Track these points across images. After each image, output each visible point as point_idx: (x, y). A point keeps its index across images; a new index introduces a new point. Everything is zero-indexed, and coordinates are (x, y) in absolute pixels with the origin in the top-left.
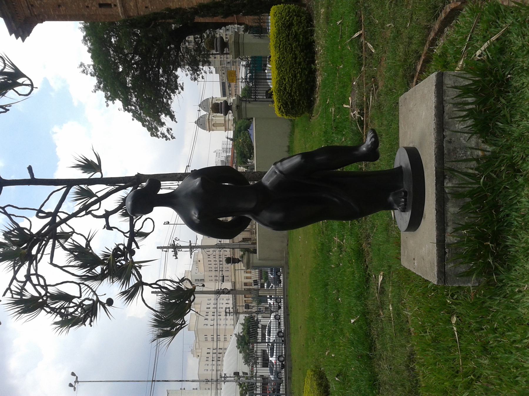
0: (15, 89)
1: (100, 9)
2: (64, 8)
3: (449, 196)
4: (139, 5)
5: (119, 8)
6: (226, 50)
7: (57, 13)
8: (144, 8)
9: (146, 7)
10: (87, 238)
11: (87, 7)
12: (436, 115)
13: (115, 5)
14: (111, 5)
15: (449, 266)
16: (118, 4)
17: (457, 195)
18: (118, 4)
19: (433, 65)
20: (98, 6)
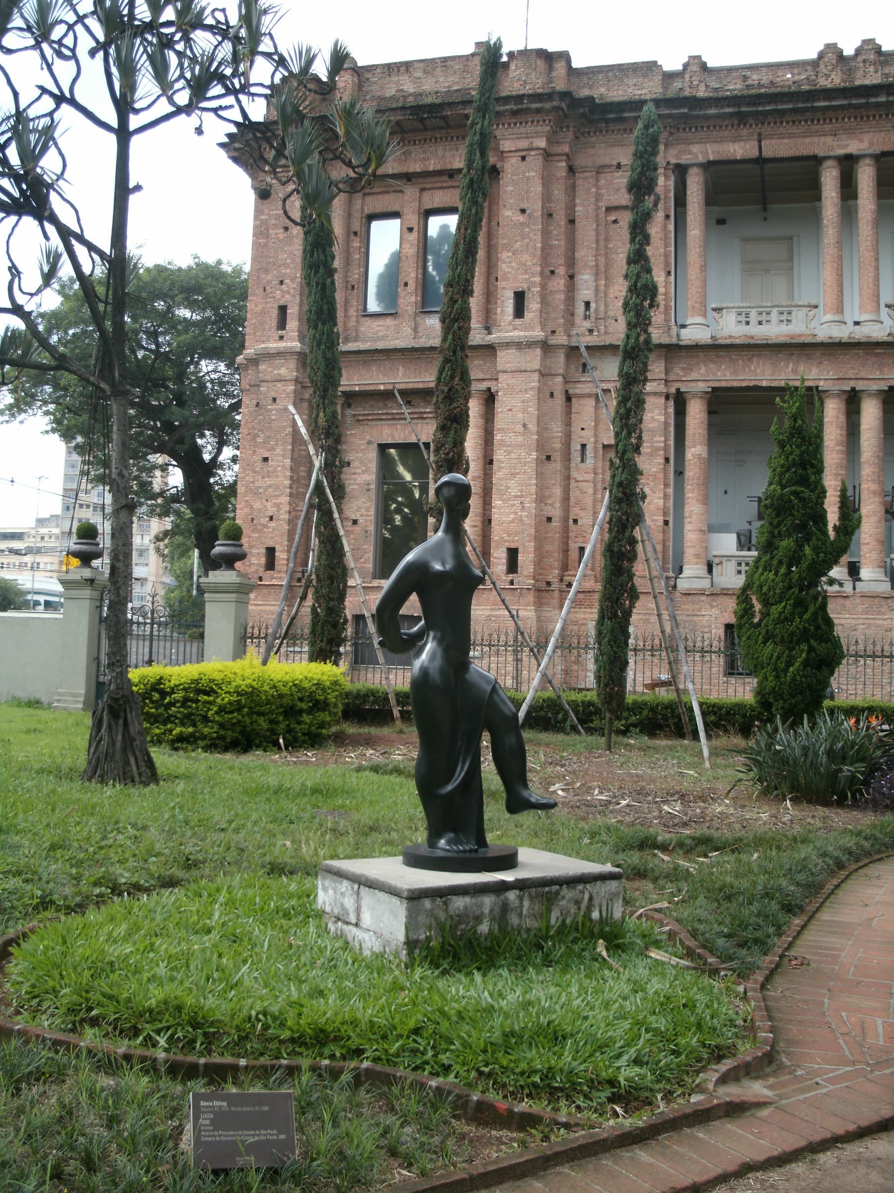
0: (9, 26)
1: (276, 306)
2: (281, 236)
3: (502, 897)
4: (279, 385)
5: (275, 345)
6: (75, 562)
7: (273, 222)
8: (273, 395)
9: (274, 400)
10: (9, 306)
11: (282, 282)
12: (583, 874)
13: (281, 338)
14: (394, 395)
15: (427, 904)
16: (284, 344)
17: (505, 908)
18: (284, 344)
19: (857, 722)
20: (282, 303)
